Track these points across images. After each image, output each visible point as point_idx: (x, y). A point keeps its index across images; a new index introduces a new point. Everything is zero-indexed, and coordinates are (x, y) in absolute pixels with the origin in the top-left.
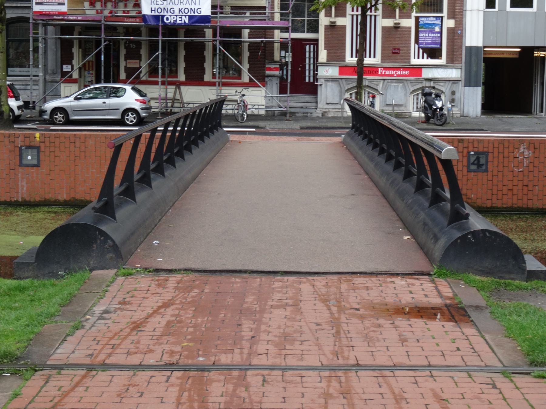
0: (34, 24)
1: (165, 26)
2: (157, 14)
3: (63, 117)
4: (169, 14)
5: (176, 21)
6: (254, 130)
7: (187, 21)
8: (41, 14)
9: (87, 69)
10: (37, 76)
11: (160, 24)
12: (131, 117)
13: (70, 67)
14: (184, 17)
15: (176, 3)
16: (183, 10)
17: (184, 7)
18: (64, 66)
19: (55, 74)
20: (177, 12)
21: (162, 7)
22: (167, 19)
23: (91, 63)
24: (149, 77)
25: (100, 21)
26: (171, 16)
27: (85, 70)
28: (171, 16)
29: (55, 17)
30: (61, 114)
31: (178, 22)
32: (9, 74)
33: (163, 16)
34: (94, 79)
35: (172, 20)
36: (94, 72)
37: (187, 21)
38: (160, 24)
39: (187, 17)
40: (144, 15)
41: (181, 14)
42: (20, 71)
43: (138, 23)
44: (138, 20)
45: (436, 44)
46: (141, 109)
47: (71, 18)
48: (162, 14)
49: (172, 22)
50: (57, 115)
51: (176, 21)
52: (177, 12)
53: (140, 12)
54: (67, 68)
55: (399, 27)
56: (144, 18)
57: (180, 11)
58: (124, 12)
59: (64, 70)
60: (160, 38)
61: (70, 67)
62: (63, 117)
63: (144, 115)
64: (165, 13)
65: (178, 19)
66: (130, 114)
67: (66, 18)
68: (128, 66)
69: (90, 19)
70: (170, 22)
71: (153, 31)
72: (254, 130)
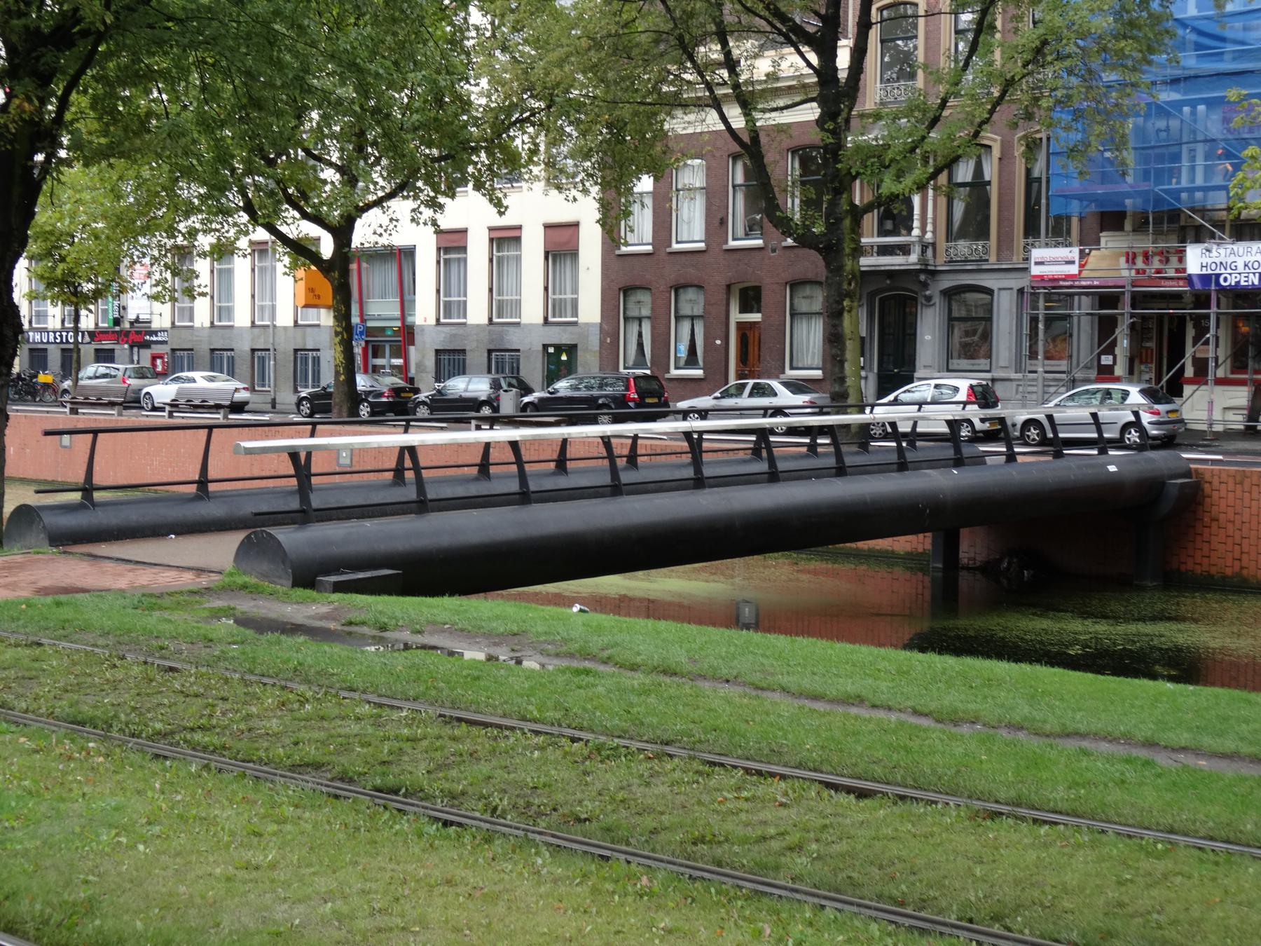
0: (1032, 294)
1: (1222, 290)
2: (1210, 272)
3: (1038, 435)
4: (1229, 271)
5: (1239, 282)
6: (1220, 457)
7: (1256, 282)
8: (1041, 278)
9: (1144, 360)
10: (1035, 372)
11: (1213, 287)
12: (1033, 433)
13: (1111, 357)
14: (1251, 275)
15: (1241, 254)
16: (1250, 265)
17: (1252, 259)
18: (1103, 357)
19: (1089, 368)
20: (1241, 268)
21: (1218, 261)
22: (1225, 280)
23: (1149, 352)
24: (1233, 373)
25: (1123, 287)
26: (1230, 274)
27: (1141, 362)
28: (1230, 274)
29: (1062, 283)
30: (1035, 429)
31: (1243, 283)
32: (951, 367)
33: (1218, 276)
34: (1153, 376)
35: (1232, 281)
36: (1153, 366)
37: (1256, 282)
38: (1213, 287)
39: (1257, 275)
40: (1190, 275)
41: (1247, 270)
42: (973, 365)
43: (1182, 288)
44: (1181, 283)
45: (1092, 322)
46: (1149, 423)
47: (1084, 283)
48: (1218, 271)
49: (1233, 284)
50: (1029, 430)
51: (1239, 282)
52: (1241, 268)
53: (1184, 270)
54: (1106, 360)
55: (232, 327)
56: (1189, 279)
57: (1246, 265)
58: (1177, 271)
59: (1103, 363)
60: (1214, 309)
61: (1111, 357)
62: (1038, 435)
63: (1155, 432)
64: (1223, 271)
65: (1243, 279)
66: (1133, 431)
67: (1077, 283)
68: (1198, 355)
69: (1110, 284)
70: (1230, 285)
71: (1202, 300)
72: (1220, 457)
